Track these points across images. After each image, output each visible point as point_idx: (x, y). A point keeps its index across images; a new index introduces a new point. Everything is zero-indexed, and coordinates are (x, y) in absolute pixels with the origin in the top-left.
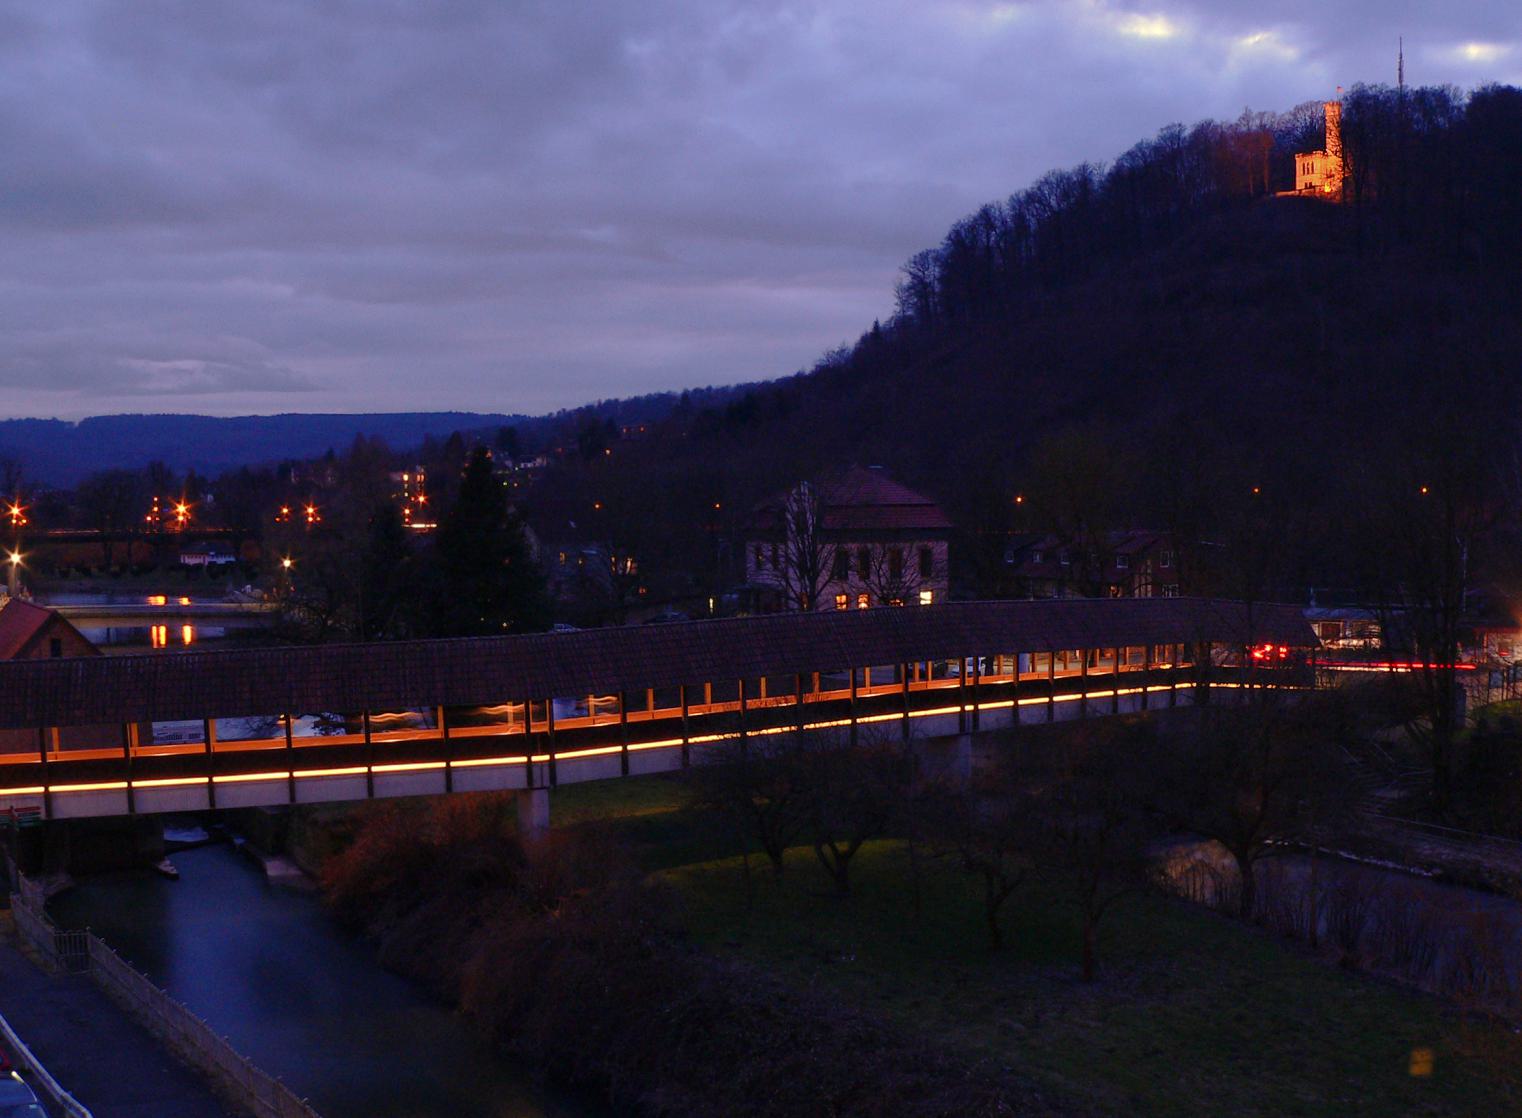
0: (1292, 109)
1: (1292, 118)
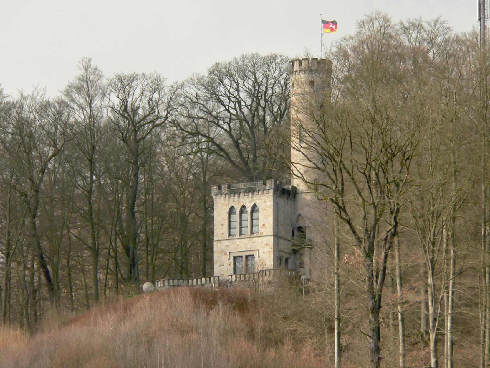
0: (204, 73)
1: (202, 92)
